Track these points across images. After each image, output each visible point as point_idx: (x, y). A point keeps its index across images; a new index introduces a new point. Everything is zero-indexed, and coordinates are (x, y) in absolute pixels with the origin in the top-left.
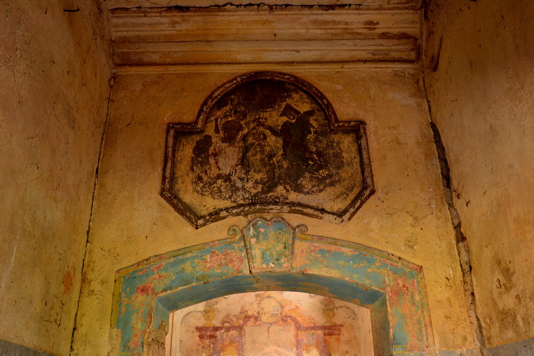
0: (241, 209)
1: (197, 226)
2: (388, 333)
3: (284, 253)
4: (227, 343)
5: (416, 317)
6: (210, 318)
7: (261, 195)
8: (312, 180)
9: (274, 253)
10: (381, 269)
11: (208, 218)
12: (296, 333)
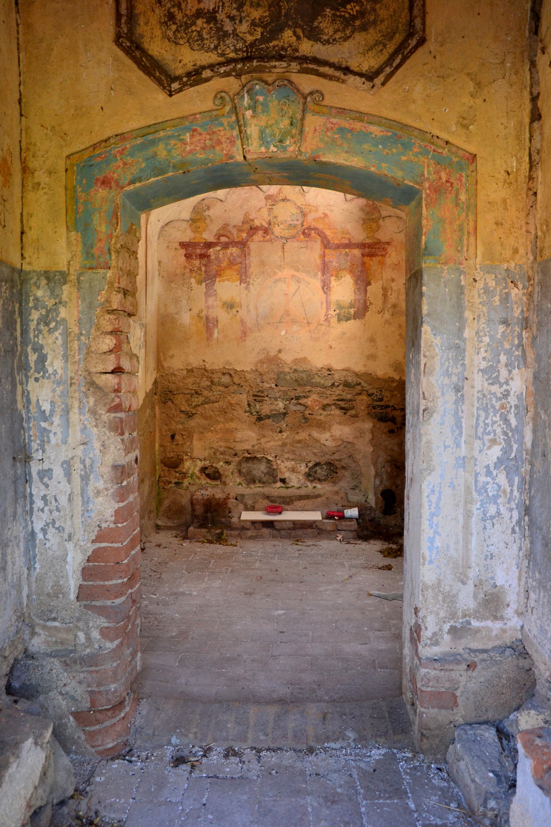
0: (231, 67)
1: (170, 91)
2: (420, 242)
3: (291, 131)
4: (224, 264)
5: (458, 222)
6: (200, 230)
7: (259, 45)
8: (335, 20)
9: (277, 131)
10: (420, 157)
11: (185, 79)
12: (322, 252)
